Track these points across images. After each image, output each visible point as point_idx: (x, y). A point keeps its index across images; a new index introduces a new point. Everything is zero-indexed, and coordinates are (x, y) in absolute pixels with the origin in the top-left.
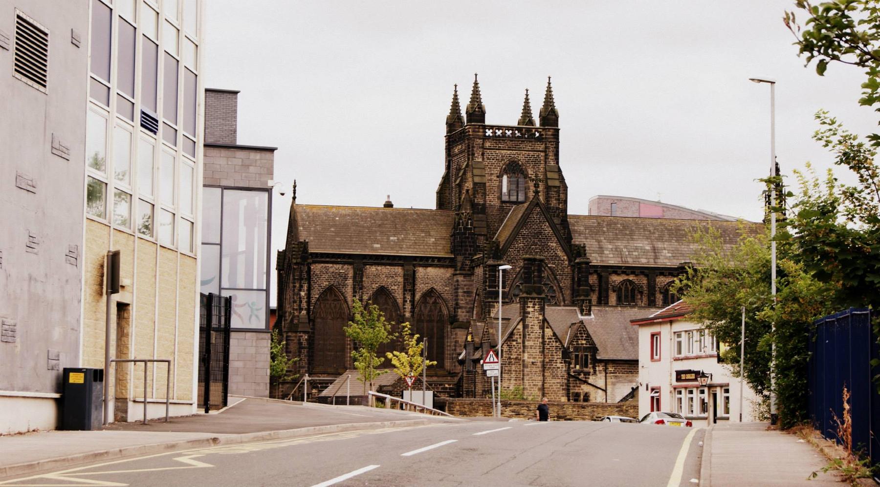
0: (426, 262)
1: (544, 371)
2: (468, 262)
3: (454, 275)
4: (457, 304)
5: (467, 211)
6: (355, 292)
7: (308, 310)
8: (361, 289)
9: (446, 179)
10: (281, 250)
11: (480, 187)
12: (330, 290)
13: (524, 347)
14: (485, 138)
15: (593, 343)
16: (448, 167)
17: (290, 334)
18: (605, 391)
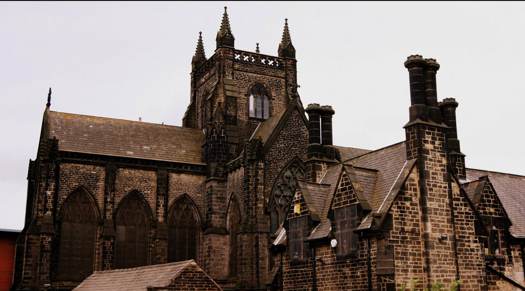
0: (180, 168)
1: (456, 254)
3: (206, 182)
4: (210, 209)
5: (219, 121)
6: (106, 194)
7: (54, 211)
9: (192, 109)
11: (231, 101)
12: (79, 190)
13: (425, 210)
14: (235, 61)
15: (504, 213)
16: (194, 98)
17: (32, 236)
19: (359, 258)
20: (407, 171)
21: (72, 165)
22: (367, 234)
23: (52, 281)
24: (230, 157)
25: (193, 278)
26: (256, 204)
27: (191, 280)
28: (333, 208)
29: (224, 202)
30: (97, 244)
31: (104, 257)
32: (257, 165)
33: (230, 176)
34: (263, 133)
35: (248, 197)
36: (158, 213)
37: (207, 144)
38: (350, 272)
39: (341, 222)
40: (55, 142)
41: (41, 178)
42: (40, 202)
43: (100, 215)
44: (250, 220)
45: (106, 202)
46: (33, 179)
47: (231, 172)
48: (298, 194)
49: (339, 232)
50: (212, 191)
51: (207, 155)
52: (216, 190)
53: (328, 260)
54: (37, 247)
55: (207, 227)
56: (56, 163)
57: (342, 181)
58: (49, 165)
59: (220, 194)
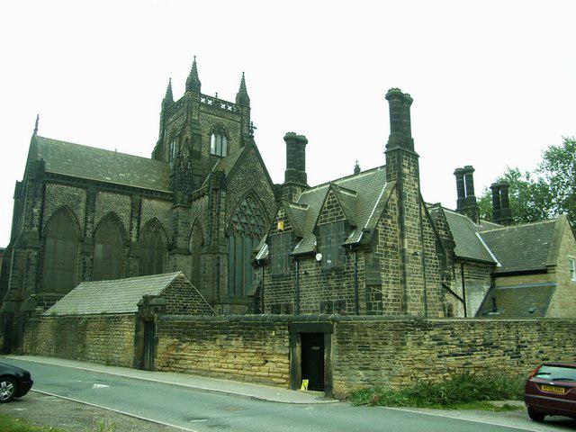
0: (151, 194)
2: (186, 197)
5: (186, 155)
6: (87, 214)
7: (40, 228)
8: (93, 212)
10: (20, 181)
11: (197, 137)
12: (63, 210)
13: (402, 228)
15: (451, 236)
18: (463, 301)
20: (389, 192)
22: (356, 248)
23: (37, 292)
24: (194, 187)
26: (218, 229)
31: (84, 272)
40: (42, 164)
45: (86, 221)
55: (172, 248)
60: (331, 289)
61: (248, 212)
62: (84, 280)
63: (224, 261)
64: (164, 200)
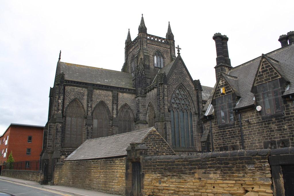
0: (123, 90)
2: (143, 91)
4: (138, 111)
5: (141, 67)
6: (88, 102)
11: (147, 57)
12: (75, 100)
16: (126, 59)
19: (285, 116)
21: (71, 87)
24: (147, 85)
25: (155, 138)
26: (164, 107)
27: (154, 140)
28: (255, 85)
29: (145, 108)
30: (84, 128)
32: (164, 86)
33: (148, 94)
34: (167, 71)
35: (160, 103)
36: (113, 113)
37: (135, 79)
38: (276, 127)
39: (262, 94)
41: (56, 93)
42: (55, 106)
43: (85, 113)
44: (161, 115)
45: (88, 106)
46: (52, 97)
47: (148, 92)
48: (222, 81)
49: (262, 100)
50: (139, 101)
51: (136, 84)
52: (141, 101)
53: (253, 121)
54: (54, 129)
56: (63, 86)
57: (263, 65)
58: (60, 87)
59: (143, 104)
60: (273, 131)
61: (180, 97)
62: (87, 139)
63: (169, 126)
64: (130, 93)
